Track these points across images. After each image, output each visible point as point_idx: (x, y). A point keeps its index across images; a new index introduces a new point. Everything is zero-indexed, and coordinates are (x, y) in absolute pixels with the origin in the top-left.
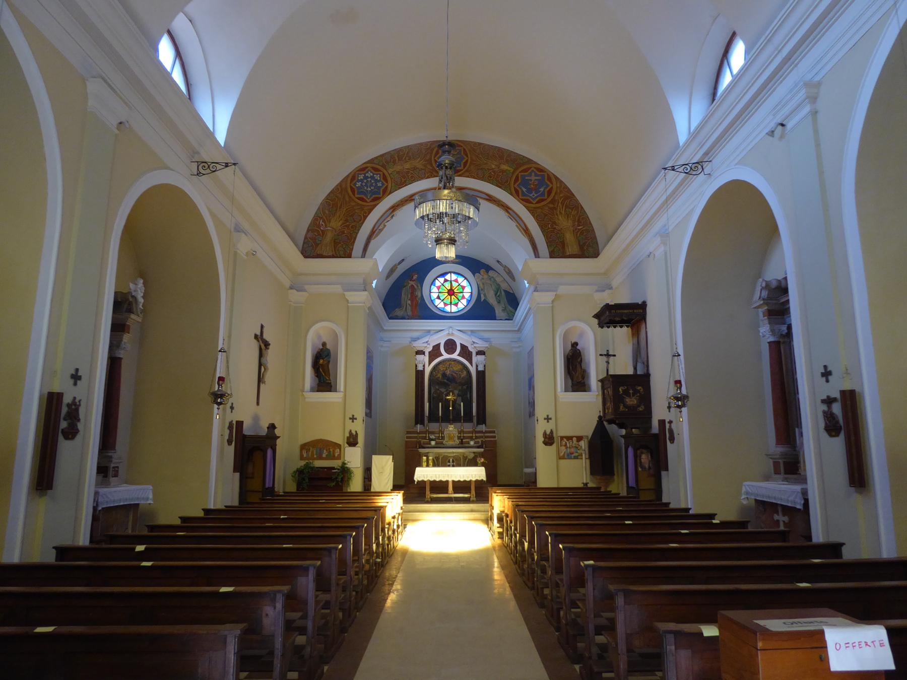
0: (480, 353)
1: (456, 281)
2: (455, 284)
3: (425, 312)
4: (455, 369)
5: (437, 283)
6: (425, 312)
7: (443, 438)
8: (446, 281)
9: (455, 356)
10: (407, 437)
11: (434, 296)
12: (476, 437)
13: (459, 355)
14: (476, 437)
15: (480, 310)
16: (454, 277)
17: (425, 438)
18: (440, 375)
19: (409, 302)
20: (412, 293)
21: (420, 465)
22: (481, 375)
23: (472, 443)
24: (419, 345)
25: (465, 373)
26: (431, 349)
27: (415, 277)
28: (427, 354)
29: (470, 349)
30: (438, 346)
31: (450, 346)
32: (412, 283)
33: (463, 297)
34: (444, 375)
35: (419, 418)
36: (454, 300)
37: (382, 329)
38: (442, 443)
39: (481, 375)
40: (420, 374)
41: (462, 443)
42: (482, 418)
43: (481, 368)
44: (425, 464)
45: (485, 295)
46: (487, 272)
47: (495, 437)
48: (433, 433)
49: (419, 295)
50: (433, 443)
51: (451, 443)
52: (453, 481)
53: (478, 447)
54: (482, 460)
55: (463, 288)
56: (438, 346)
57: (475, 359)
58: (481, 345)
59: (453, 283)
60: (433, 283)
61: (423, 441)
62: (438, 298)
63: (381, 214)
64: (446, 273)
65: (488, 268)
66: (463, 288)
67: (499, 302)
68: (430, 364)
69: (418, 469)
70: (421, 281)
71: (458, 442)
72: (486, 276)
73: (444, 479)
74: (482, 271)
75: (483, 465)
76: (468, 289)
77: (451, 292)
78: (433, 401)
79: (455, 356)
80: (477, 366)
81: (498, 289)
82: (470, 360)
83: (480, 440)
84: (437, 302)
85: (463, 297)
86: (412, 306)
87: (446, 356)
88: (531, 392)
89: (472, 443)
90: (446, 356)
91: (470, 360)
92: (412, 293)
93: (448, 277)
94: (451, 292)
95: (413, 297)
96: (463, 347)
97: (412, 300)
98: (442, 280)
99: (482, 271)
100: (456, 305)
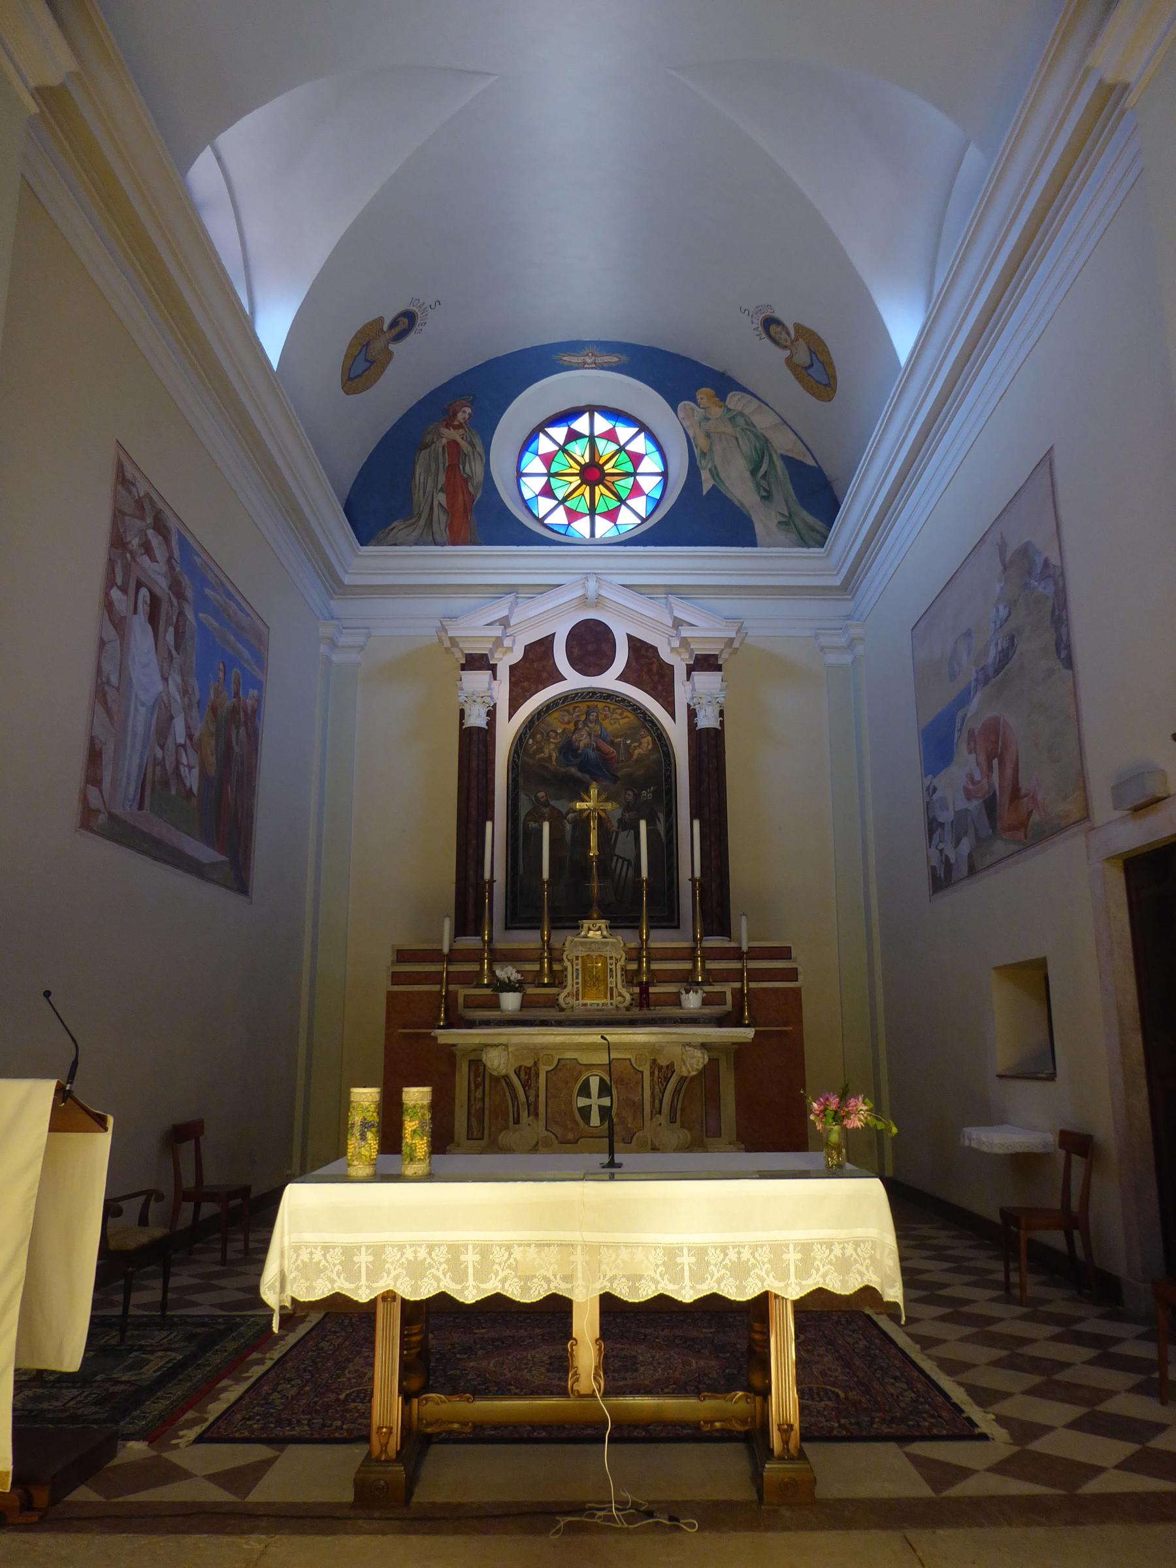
0: (705, 663)
1: (611, 436)
2: (605, 448)
3: (491, 520)
4: (610, 727)
5: (544, 445)
6: (491, 520)
7: (558, 980)
8: (573, 436)
9: (609, 680)
10: (397, 978)
11: (531, 487)
12: (712, 977)
13: (622, 677)
14: (712, 977)
15: (697, 517)
16: (602, 424)
17: (472, 979)
18: (551, 750)
19: (442, 498)
20: (453, 469)
21: (321, 1159)
22: (708, 746)
23: (692, 1001)
24: (475, 628)
25: (647, 742)
26: (517, 655)
28: (504, 673)
29: (666, 655)
30: (546, 644)
31: (591, 645)
32: (455, 435)
33: (636, 491)
34: (568, 749)
35: (469, 908)
36: (605, 502)
37: (335, 586)
38: (553, 1003)
39: (708, 746)
40: (475, 744)
41: (644, 999)
42: (716, 911)
43: (707, 720)
44: (363, 1148)
45: (714, 473)
46: (722, 396)
47: (792, 975)
48: (512, 957)
49: (478, 470)
50: (510, 1001)
51: (594, 1001)
52: (611, 1307)
53: (720, 1021)
54: (860, 1114)
55: (636, 459)
56: (546, 644)
57: (682, 693)
58: (706, 628)
59: (601, 444)
61: (463, 992)
62: (547, 492)
65: (723, 384)
66: (636, 459)
67: (767, 497)
68: (513, 708)
69: (299, 1199)
70: (485, 426)
71: (626, 995)
72: (716, 411)
73: (527, 1292)
74: (704, 394)
75: (855, 1158)
76: (652, 463)
77: (592, 474)
78: (521, 842)
79: (609, 680)
80: (692, 714)
82: (663, 690)
83: (728, 988)
84: (544, 505)
85: (636, 491)
86: (450, 510)
87: (573, 681)
89: (692, 1001)
90: (573, 681)
91: (663, 690)
92: (453, 469)
93: (581, 424)
94: (592, 474)
95: (456, 481)
96: (640, 650)
97: (450, 489)
98: (559, 433)
99: (704, 394)
100: (612, 515)
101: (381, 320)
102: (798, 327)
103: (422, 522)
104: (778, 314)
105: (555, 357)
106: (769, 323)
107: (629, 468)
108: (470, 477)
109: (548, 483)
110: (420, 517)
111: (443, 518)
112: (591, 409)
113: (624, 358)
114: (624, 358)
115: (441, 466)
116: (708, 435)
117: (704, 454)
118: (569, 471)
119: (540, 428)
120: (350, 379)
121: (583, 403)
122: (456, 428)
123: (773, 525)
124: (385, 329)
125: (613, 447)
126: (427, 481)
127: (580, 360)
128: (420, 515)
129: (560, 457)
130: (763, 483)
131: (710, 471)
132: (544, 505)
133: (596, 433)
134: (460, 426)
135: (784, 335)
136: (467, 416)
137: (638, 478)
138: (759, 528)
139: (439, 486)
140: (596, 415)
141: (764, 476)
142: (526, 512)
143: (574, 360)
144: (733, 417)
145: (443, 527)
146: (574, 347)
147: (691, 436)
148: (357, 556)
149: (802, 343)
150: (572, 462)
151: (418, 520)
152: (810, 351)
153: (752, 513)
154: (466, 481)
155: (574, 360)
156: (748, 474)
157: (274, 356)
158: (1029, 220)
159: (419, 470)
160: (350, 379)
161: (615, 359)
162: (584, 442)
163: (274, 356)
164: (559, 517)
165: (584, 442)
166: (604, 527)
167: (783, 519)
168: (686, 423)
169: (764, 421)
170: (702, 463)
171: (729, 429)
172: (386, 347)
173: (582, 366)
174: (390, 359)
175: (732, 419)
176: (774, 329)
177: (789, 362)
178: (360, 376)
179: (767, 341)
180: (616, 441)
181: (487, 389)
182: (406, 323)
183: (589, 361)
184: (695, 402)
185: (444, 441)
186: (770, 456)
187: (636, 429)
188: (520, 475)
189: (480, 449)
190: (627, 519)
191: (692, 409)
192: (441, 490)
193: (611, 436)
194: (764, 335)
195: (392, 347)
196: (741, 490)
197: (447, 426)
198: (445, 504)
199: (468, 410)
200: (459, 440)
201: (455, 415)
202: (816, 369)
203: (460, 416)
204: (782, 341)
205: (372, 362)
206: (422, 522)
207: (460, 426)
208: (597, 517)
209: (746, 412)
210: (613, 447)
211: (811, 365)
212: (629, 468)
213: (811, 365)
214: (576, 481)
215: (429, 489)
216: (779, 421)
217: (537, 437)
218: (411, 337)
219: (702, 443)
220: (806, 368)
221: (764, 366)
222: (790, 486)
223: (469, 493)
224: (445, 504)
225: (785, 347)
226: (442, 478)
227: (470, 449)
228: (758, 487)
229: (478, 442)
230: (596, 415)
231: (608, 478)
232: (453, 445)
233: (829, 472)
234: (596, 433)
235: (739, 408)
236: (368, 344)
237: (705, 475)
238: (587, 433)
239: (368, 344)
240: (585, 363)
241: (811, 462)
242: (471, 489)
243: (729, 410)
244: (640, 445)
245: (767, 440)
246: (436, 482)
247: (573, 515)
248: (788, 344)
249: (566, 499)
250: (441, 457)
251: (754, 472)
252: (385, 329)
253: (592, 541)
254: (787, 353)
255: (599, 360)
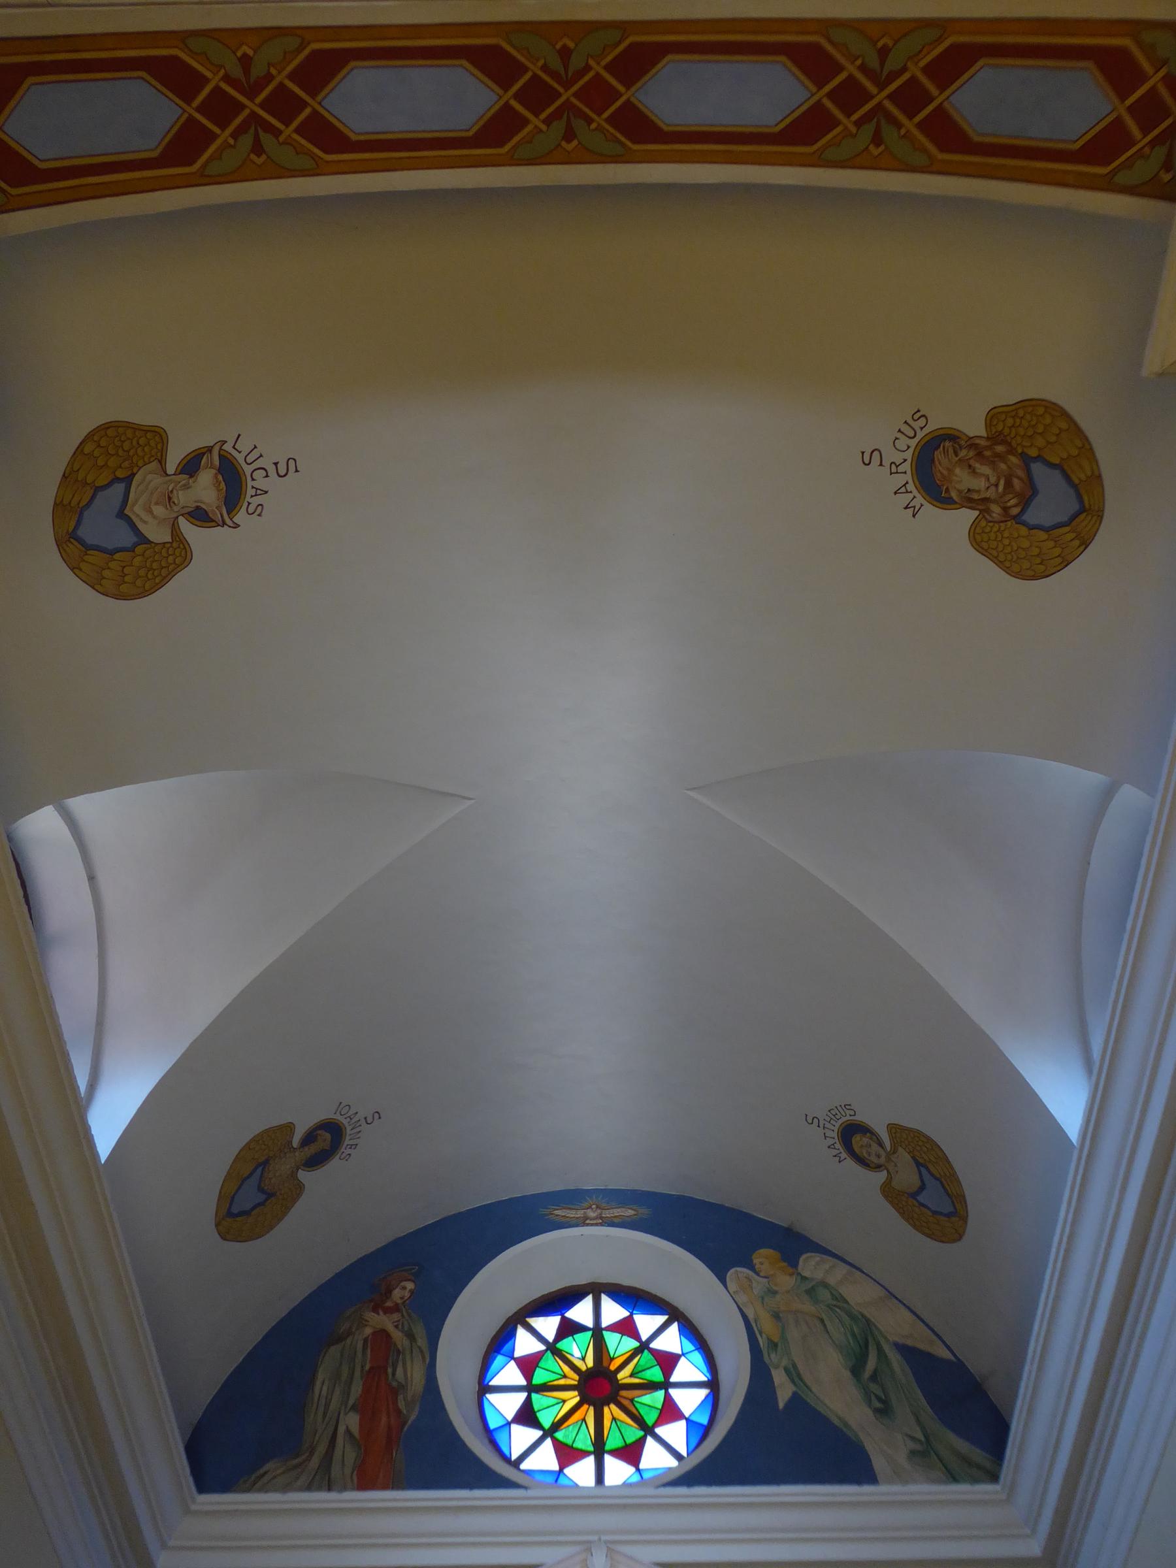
8: (568, 1329)
19: (352, 1421)
20: (377, 1375)
27: (403, 1291)
32: (386, 1322)
33: (670, 1412)
36: (620, 1432)
49: (416, 1376)
55: (668, 1362)
60: (501, 1341)
62: (527, 1416)
63: (38, 210)
64: (571, 1296)
65: (791, 1244)
66: (668, 1362)
67: (884, 1410)
70: (434, 1309)
72: (785, 1281)
74: (764, 1257)
77: (599, 1386)
81: (862, 1347)
85: (670, 1412)
88: (982, 100)
92: (377, 1375)
93: (582, 1312)
94: (599, 1386)
97: (367, 1409)
98: (548, 1325)
99: (764, 1257)
100: (631, 1454)
101: (289, 1128)
102: (893, 1129)
103: (315, 1462)
104: (863, 1117)
105: (543, 1211)
106: (852, 1134)
107: (656, 1374)
108: (402, 1387)
109: (528, 1403)
110: (312, 1453)
111: (351, 1455)
112: (596, 1290)
113: (644, 1212)
114: (644, 1212)
115: (358, 1374)
116: (776, 1316)
117: (773, 1345)
118: (562, 1382)
119: (521, 1317)
120: (230, 1214)
121: (582, 1280)
122: (388, 1311)
123: (902, 1458)
124: (295, 1143)
125: (630, 1344)
126: (333, 1398)
127: (580, 1214)
128: (312, 1451)
129: (549, 1362)
130: (873, 1387)
131: (786, 1370)
132: (521, 1438)
133: (604, 1324)
134: (396, 1309)
135: (875, 1147)
136: (407, 1295)
137: (672, 1391)
138: (879, 1463)
139: (351, 1402)
140: (604, 1298)
141: (874, 1377)
142: (490, 1447)
143: (572, 1214)
144: (813, 1288)
145: (348, 1471)
146: (572, 1197)
147: (751, 1316)
148: (187, 1512)
149: (904, 1156)
150: (566, 1369)
151: (309, 1459)
152: (918, 1164)
153: (862, 1436)
154: (395, 1392)
155: (572, 1214)
156: (847, 1374)
157: (105, 1145)
158: (1140, 1204)
159: (320, 1376)
160: (230, 1214)
161: (632, 1212)
162: (585, 1338)
163: (105, 1145)
164: (545, 1459)
165: (585, 1338)
166: (617, 1472)
167: (918, 1447)
168: (742, 1299)
169: (859, 1294)
170: (771, 1358)
171: (808, 1307)
172: (293, 1175)
173: (583, 1222)
174: (299, 1195)
175: (811, 1292)
176: (858, 1141)
177: (889, 1192)
178: (246, 1213)
179: (850, 1163)
180: (635, 1334)
181: (438, 1256)
182: (327, 1141)
183: (592, 1214)
184: (752, 1267)
185: (368, 1331)
186: (880, 1350)
187: (665, 1318)
188: (484, 1389)
189: (422, 1342)
190: (655, 1458)
191: (749, 1279)
192: (353, 1408)
193: (626, 1327)
194: (844, 1155)
195: (302, 1175)
196: (840, 1400)
197: (375, 1310)
198: (355, 1430)
199: (410, 1286)
200: (390, 1328)
201: (389, 1292)
202: (928, 1188)
203: (397, 1294)
204: (874, 1159)
205: (270, 1195)
206: (315, 1462)
207: (396, 1309)
208: (590, 1324)
209: (832, 1281)
210: (630, 1344)
211: (922, 1187)
212: (656, 1374)
213: (922, 1187)
214: (573, 1398)
215: (334, 1405)
216: (883, 1293)
217: (512, 1335)
218: (335, 1163)
219: (767, 1326)
220: (914, 1195)
221: (848, 1204)
222: (919, 1392)
223: (399, 1412)
224: (355, 1430)
225: (878, 1167)
226: (357, 1389)
227: (406, 1342)
228: (868, 1396)
229: (420, 1331)
230: (604, 1298)
231: (624, 1393)
232: (382, 1336)
233: (977, 1364)
234: (604, 1324)
235: (819, 1275)
236: (265, 1163)
237: (779, 1377)
238: (590, 1323)
239: (265, 1163)
240: (587, 1218)
241: (945, 1354)
242: (401, 1404)
243: (804, 1278)
244: (671, 1340)
245: (868, 1321)
246: (347, 1394)
247: (567, 1455)
248: (882, 1160)
249: (557, 1426)
250: (359, 1354)
251: (856, 1371)
252: (295, 1143)
253: (601, 1499)
254: (882, 1176)
255: (607, 1214)
